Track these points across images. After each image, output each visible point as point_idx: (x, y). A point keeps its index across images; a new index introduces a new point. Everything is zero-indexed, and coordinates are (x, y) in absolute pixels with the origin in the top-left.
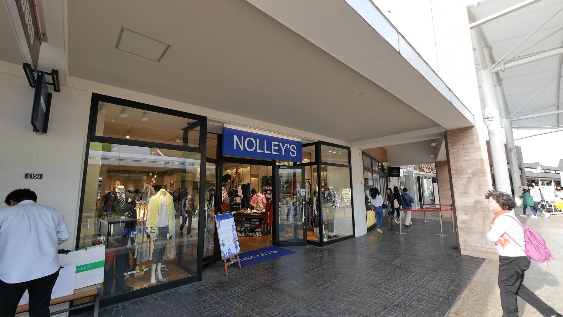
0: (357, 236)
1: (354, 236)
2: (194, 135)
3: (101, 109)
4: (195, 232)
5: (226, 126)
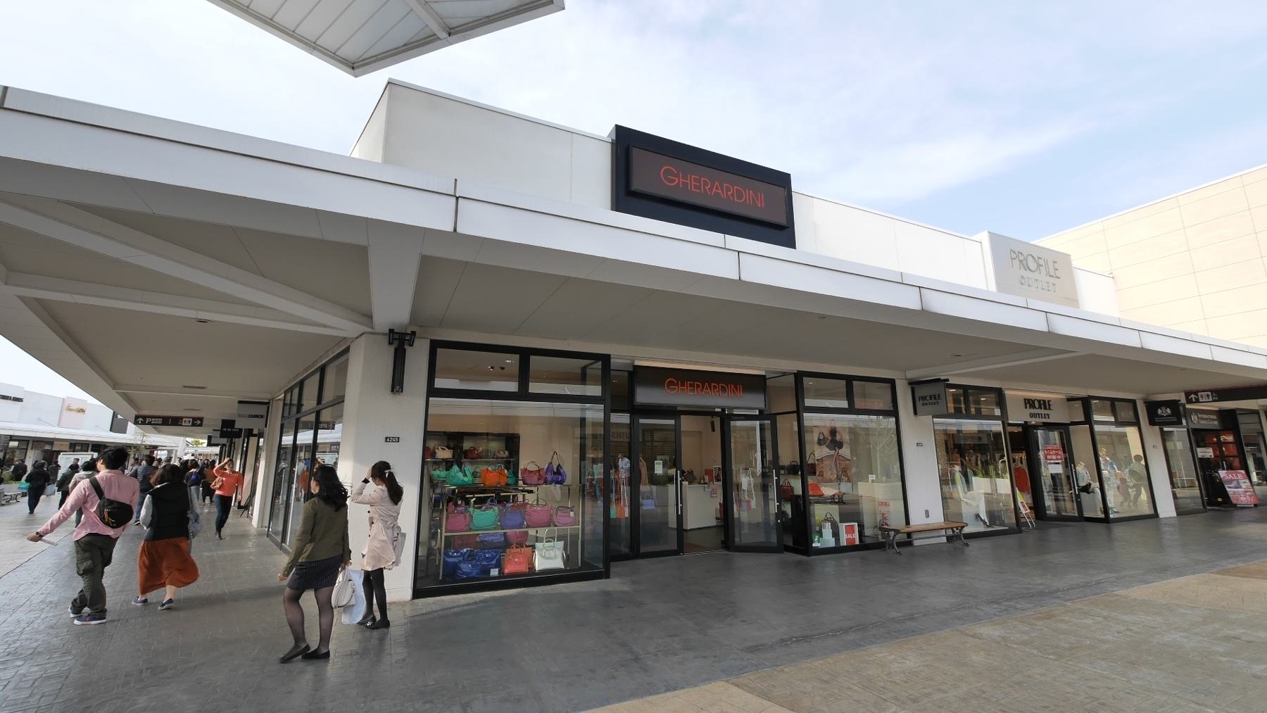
0: (1161, 515)
1: (1156, 515)
5: (637, 363)
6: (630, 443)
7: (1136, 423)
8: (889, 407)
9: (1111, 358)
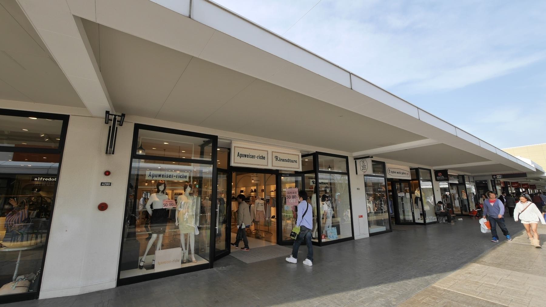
0: (356, 238)
1: (353, 238)
2: (209, 149)
3: (478, 263)
4: (209, 220)
6: (433, 188)
7: (431, 181)
8: (345, 171)
9: (331, 105)
